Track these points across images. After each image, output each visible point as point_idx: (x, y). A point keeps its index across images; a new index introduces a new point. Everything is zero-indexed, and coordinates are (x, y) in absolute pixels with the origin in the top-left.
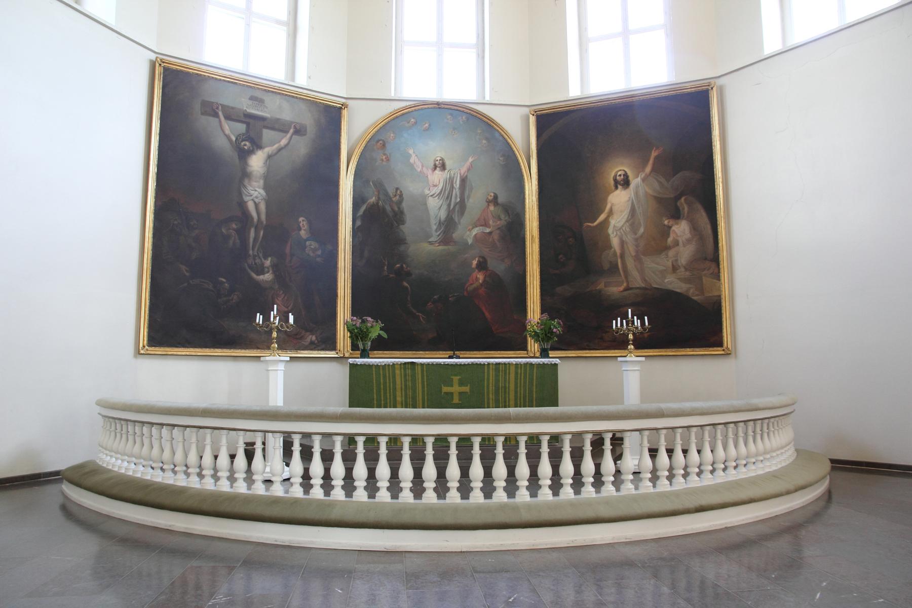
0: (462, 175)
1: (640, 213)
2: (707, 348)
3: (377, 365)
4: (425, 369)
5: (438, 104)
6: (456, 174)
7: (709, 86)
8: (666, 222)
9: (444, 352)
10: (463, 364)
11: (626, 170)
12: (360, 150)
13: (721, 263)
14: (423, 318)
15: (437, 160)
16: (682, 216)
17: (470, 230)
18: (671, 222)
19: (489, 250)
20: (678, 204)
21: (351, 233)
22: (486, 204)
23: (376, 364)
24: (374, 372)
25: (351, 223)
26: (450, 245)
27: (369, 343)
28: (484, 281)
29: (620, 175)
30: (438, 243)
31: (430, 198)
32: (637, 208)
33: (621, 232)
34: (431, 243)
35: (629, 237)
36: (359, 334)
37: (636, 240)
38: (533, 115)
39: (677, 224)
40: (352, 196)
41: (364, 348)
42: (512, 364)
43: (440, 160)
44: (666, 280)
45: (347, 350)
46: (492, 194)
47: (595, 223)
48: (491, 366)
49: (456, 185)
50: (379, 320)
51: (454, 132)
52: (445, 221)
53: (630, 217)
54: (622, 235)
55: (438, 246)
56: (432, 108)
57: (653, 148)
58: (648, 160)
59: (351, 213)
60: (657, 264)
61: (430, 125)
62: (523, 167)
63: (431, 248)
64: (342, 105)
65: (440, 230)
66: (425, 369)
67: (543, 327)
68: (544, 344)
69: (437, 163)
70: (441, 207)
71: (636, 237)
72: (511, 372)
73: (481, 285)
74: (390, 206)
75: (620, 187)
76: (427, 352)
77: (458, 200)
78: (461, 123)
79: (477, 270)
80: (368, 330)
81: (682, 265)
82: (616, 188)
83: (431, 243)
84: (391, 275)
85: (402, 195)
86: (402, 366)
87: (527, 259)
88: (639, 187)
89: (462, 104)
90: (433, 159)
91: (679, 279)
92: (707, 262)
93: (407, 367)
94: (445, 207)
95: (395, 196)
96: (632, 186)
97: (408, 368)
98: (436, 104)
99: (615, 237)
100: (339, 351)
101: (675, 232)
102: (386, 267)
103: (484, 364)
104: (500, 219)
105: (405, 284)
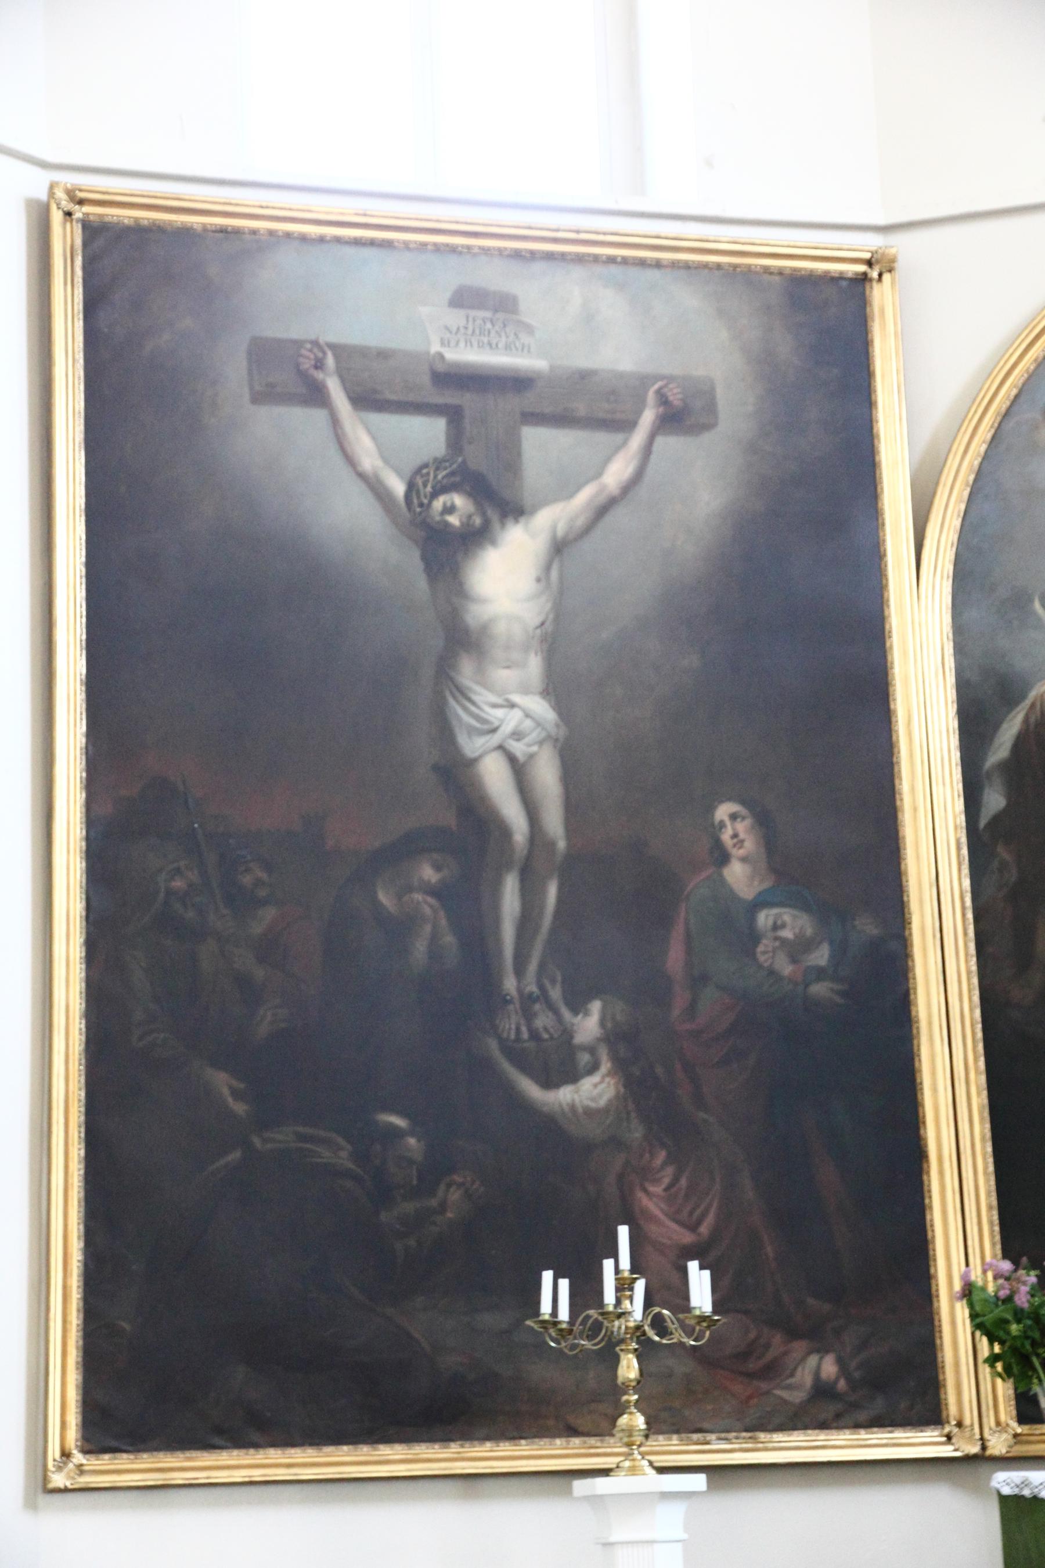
21: (965, 851)
25: (960, 805)
36: (1034, 1344)
40: (951, 680)
45: (998, 1423)
64: (869, 263)
100: (960, 1425)
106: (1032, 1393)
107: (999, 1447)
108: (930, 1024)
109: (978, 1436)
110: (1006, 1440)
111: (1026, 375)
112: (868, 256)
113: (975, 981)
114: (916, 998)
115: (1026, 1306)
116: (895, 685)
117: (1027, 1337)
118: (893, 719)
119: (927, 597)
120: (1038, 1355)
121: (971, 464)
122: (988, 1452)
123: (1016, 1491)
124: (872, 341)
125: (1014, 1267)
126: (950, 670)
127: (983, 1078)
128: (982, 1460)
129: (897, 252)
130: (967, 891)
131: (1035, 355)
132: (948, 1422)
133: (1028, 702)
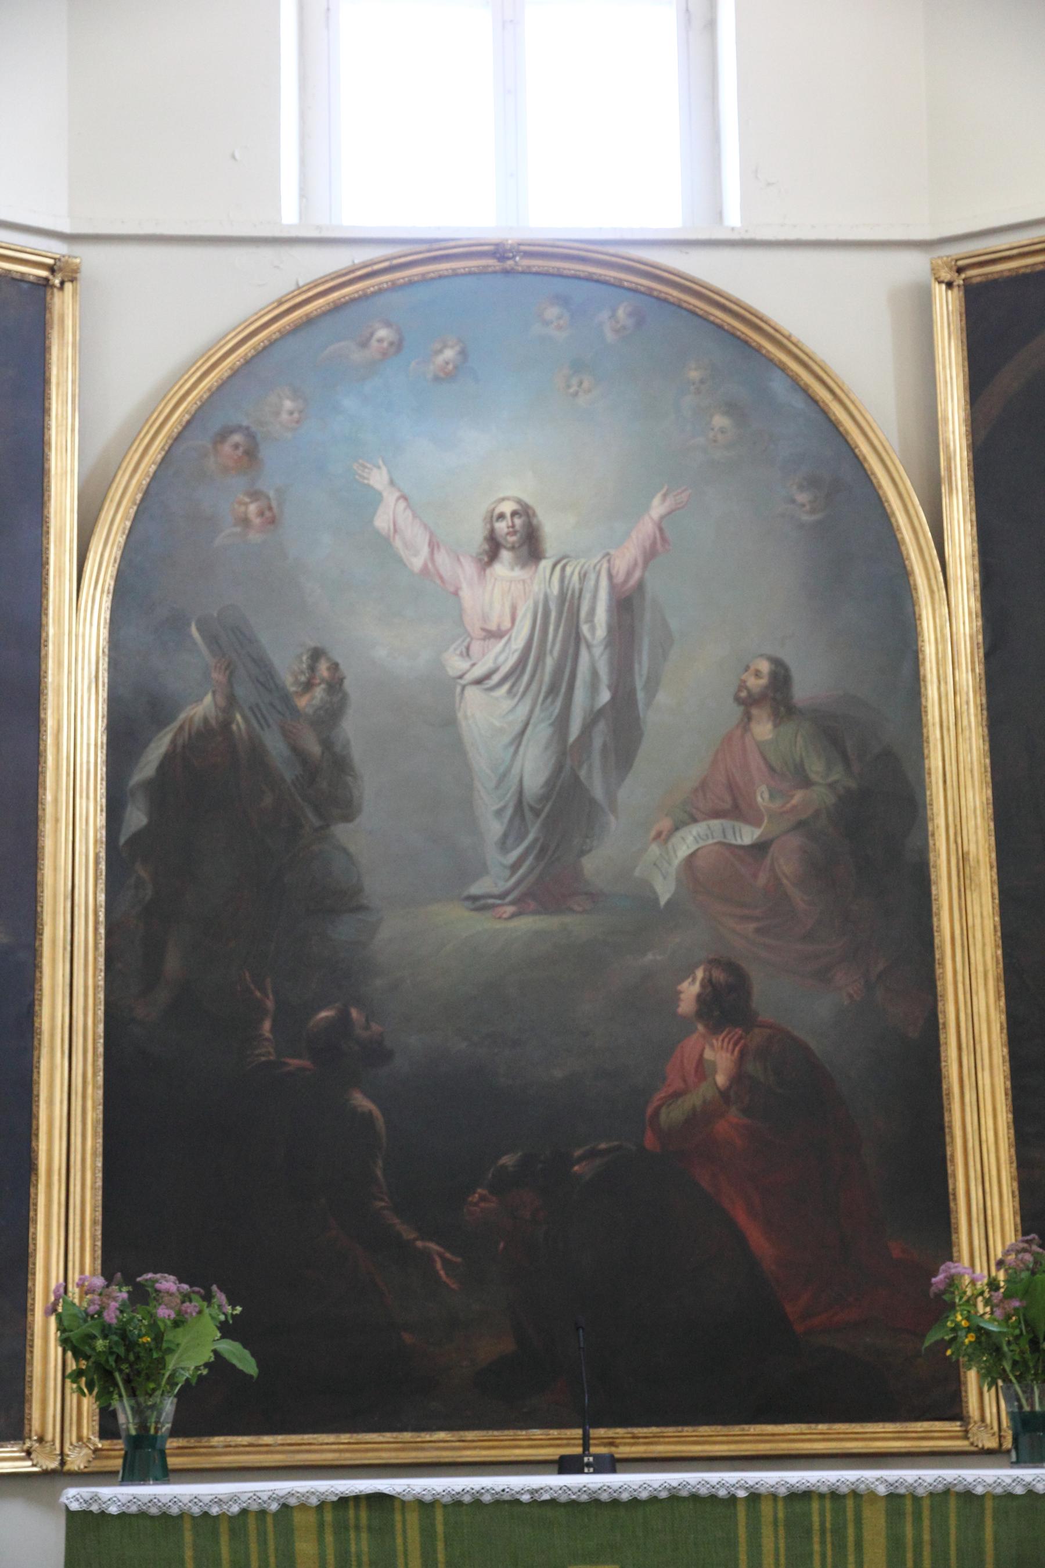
0: (619, 578)
3: (206, 1514)
4: (440, 1528)
5: (500, 252)
6: (592, 576)
9: (554, 1433)
10: (625, 1496)
12: (141, 479)
14: (445, 1262)
15: (501, 516)
17: (663, 838)
19: (758, 931)
21: (103, 866)
22: (739, 710)
23: (196, 1510)
24: (189, 1553)
25: (102, 820)
26: (572, 910)
27: (169, 1406)
28: (738, 1077)
30: (512, 903)
31: (472, 693)
34: (479, 904)
36: (118, 1359)
38: (949, 285)
40: (103, 694)
41: (143, 1427)
42: (872, 1495)
43: (514, 514)
45: (80, 1438)
46: (765, 666)
48: (766, 1509)
49: (593, 629)
50: (214, 1288)
51: (574, 381)
52: (544, 798)
55: (513, 916)
56: (470, 273)
59: (102, 770)
61: (463, 353)
62: (906, 534)
63: (483, 924)
64: (52, 269)
65: (521, 838)
66: (440, 1528)
67: (1016, 1304)
68: (1028, 1391)
69: (502, 527)
70: (523, 732)
72: (867, 1536)
73: (725, 1095)
74: (286, 734)
76: (470, 1435)
77: (605, 696)
78: (610, 336)
79: (701, 1028)
80: (159, 1338)
83: (479, 904)
84: (294, 1062)
85: (341, 680)
86: (328, 1517)
87: (942, 964)
89: (612, 250)
90: (483, 509)
93: (352, 1522)
94: (541, 732)
95: (308, 686)
97: (357, 1528)
98: (492, 254)
100: (41, 1440)
102: (267, 1025)
103: (733, 1499)
104: (806, 783)
105: (361, 1101)
106: (111, 1408)
107: (78, 1462)
108: (52, 1036)
109: (58, 1452)
110: (86, 1455)
111: (199, 403)
112: (51, 262)
113: (101, 996)
114: (41, 1010)
115: (114, 1321)
116: (47, 694)
117: (112, 1353)
118: (42, 729)
119: (86, 611)
120: (121, 1371)
121: (139, 483)
122: (66, 1468)
123: (84, 1506)
124: (50, 348)
125: (106, 1283)
126: (104, 686)
127: (100, 1093)
128: (62, 1475)
129: (80, 263)
130: (101, 906)
131: (209, 385)
132: (30, 1438)
133: (176, 724)
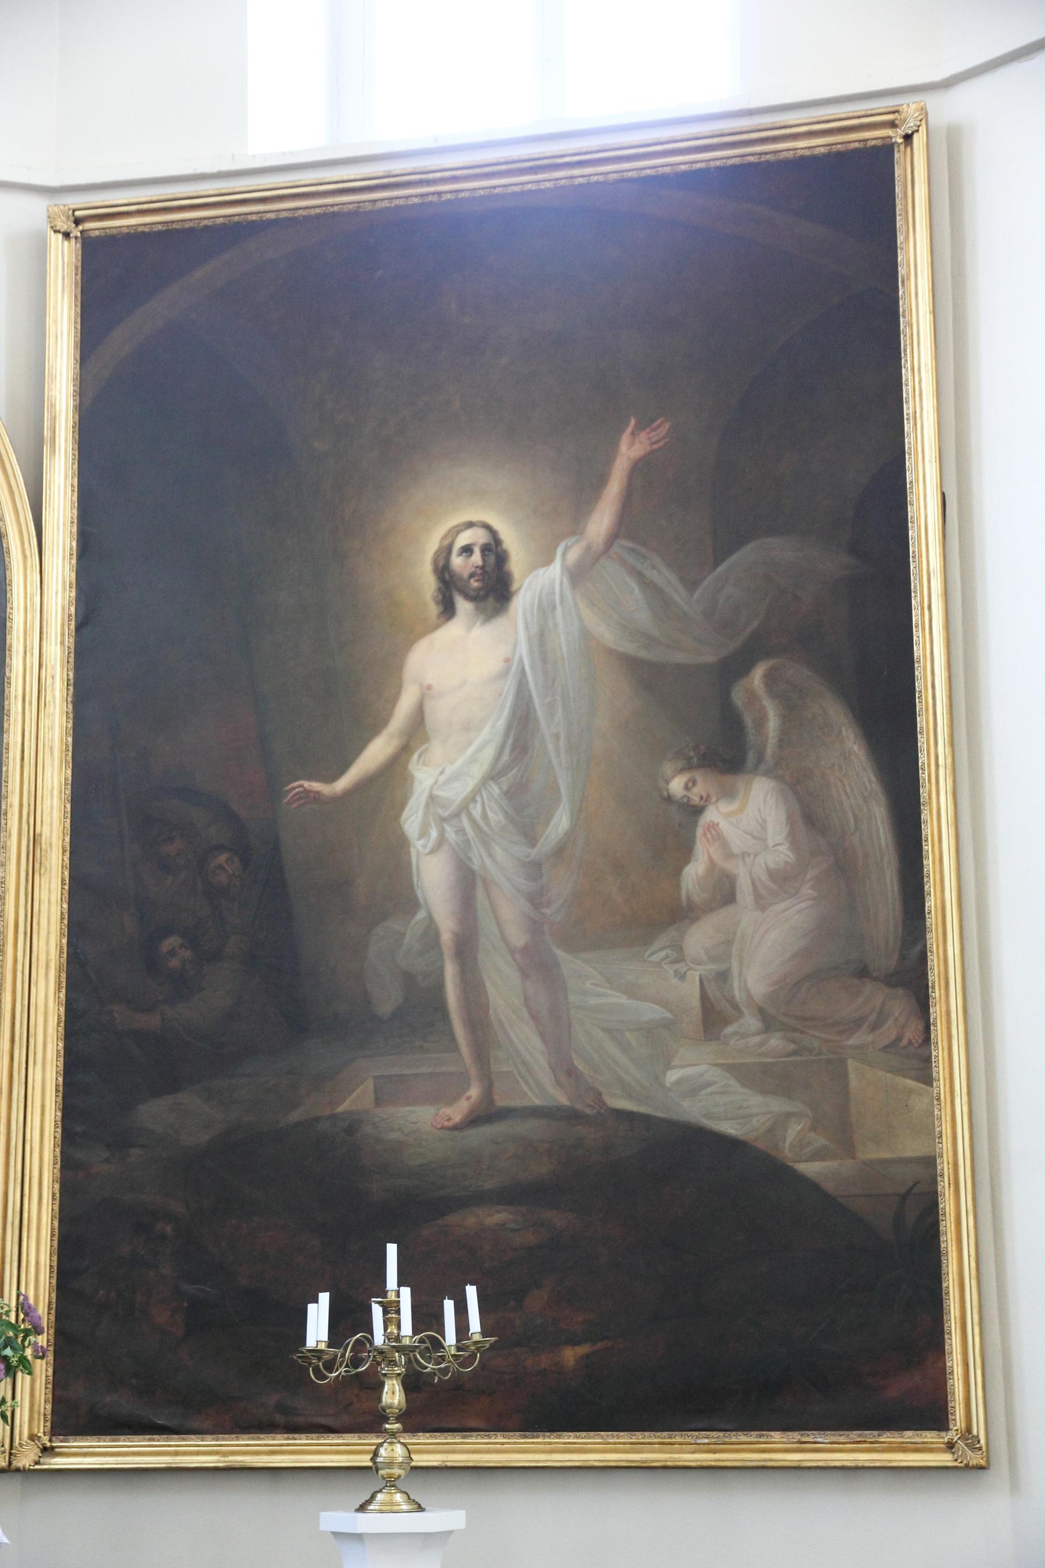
1: (557, 736)
2: (870, 1435)
7: (893, 125)
8: (677, 786)
11: (497, 524)
13: (936, 994)
16: (751, 758)
18: (703, 785)
20: (738, 696)
29: (467, 550)
32: (540, 713)
33: (461, 831)
35: (498, 851)
37: (534, 868)
38: (67, 235)
39: (729, 794)
44: (672, 1076)
47: (343, 784)
53: (505, 757)
54: (467, 841)
57: (627, 425)
58: (602, 480)
60: (632, 991)
71: (534, 852)
75: (463, 606)
81: (750, 996)
82: (448, 610)
88: (554, 608)
91: (730, 1069)
92: (869, 987)
96: (522, 602)
99: (432, 852)
101: (720, 838)
